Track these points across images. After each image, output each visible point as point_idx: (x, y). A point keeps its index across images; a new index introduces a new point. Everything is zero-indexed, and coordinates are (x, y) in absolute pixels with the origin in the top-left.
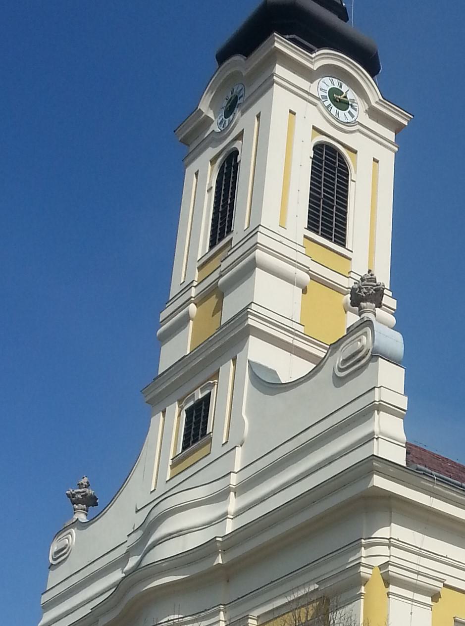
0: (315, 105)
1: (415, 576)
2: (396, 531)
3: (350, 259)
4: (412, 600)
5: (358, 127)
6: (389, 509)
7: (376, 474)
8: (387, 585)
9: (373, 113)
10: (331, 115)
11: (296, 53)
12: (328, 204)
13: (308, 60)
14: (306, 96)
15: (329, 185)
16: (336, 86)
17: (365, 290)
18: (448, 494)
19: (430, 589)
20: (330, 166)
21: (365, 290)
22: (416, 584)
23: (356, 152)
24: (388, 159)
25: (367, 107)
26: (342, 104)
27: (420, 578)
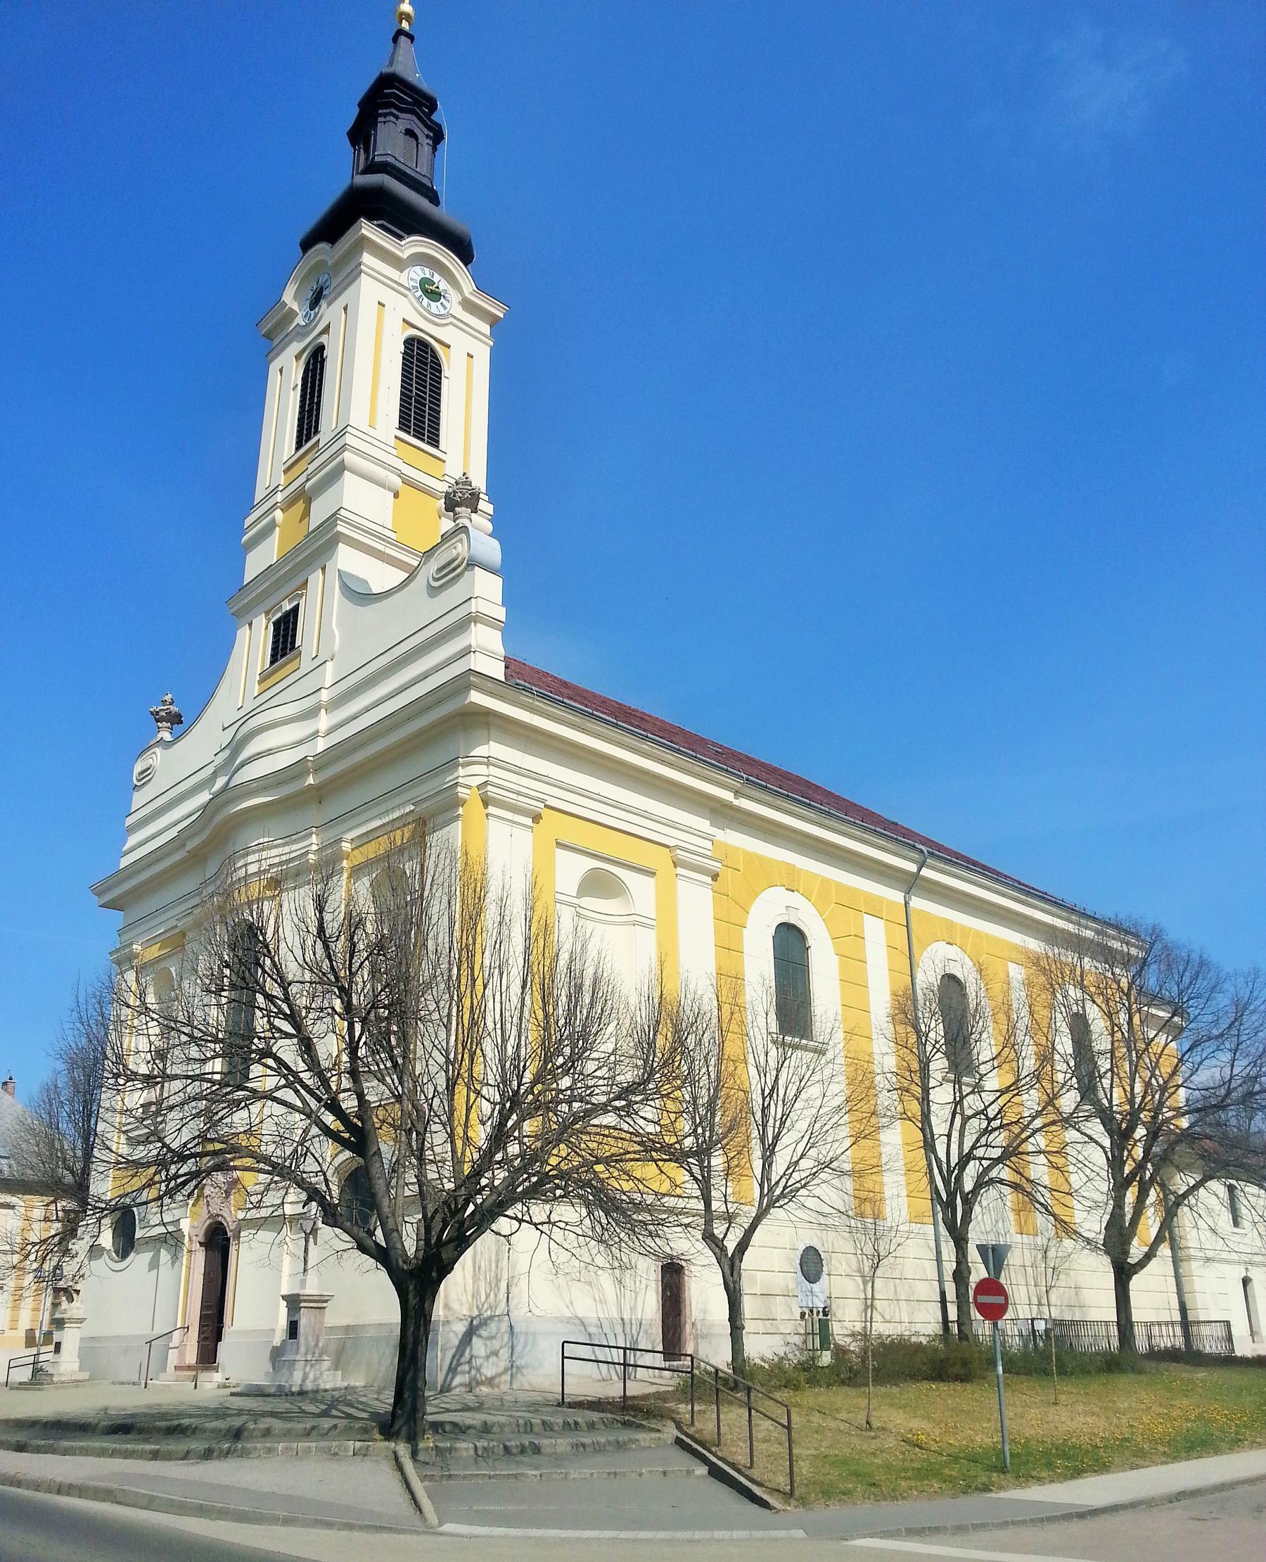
0: (405, 296)
1: (514, 796)
2: (494, 749)
3: (444, 462)
6: (488, 726)
9: (468, 305)
10: (423, 307)
15: (421, 382)
17: (460, 494)
21: (460, 494)
23: (449, 347)
27: (520, 798)
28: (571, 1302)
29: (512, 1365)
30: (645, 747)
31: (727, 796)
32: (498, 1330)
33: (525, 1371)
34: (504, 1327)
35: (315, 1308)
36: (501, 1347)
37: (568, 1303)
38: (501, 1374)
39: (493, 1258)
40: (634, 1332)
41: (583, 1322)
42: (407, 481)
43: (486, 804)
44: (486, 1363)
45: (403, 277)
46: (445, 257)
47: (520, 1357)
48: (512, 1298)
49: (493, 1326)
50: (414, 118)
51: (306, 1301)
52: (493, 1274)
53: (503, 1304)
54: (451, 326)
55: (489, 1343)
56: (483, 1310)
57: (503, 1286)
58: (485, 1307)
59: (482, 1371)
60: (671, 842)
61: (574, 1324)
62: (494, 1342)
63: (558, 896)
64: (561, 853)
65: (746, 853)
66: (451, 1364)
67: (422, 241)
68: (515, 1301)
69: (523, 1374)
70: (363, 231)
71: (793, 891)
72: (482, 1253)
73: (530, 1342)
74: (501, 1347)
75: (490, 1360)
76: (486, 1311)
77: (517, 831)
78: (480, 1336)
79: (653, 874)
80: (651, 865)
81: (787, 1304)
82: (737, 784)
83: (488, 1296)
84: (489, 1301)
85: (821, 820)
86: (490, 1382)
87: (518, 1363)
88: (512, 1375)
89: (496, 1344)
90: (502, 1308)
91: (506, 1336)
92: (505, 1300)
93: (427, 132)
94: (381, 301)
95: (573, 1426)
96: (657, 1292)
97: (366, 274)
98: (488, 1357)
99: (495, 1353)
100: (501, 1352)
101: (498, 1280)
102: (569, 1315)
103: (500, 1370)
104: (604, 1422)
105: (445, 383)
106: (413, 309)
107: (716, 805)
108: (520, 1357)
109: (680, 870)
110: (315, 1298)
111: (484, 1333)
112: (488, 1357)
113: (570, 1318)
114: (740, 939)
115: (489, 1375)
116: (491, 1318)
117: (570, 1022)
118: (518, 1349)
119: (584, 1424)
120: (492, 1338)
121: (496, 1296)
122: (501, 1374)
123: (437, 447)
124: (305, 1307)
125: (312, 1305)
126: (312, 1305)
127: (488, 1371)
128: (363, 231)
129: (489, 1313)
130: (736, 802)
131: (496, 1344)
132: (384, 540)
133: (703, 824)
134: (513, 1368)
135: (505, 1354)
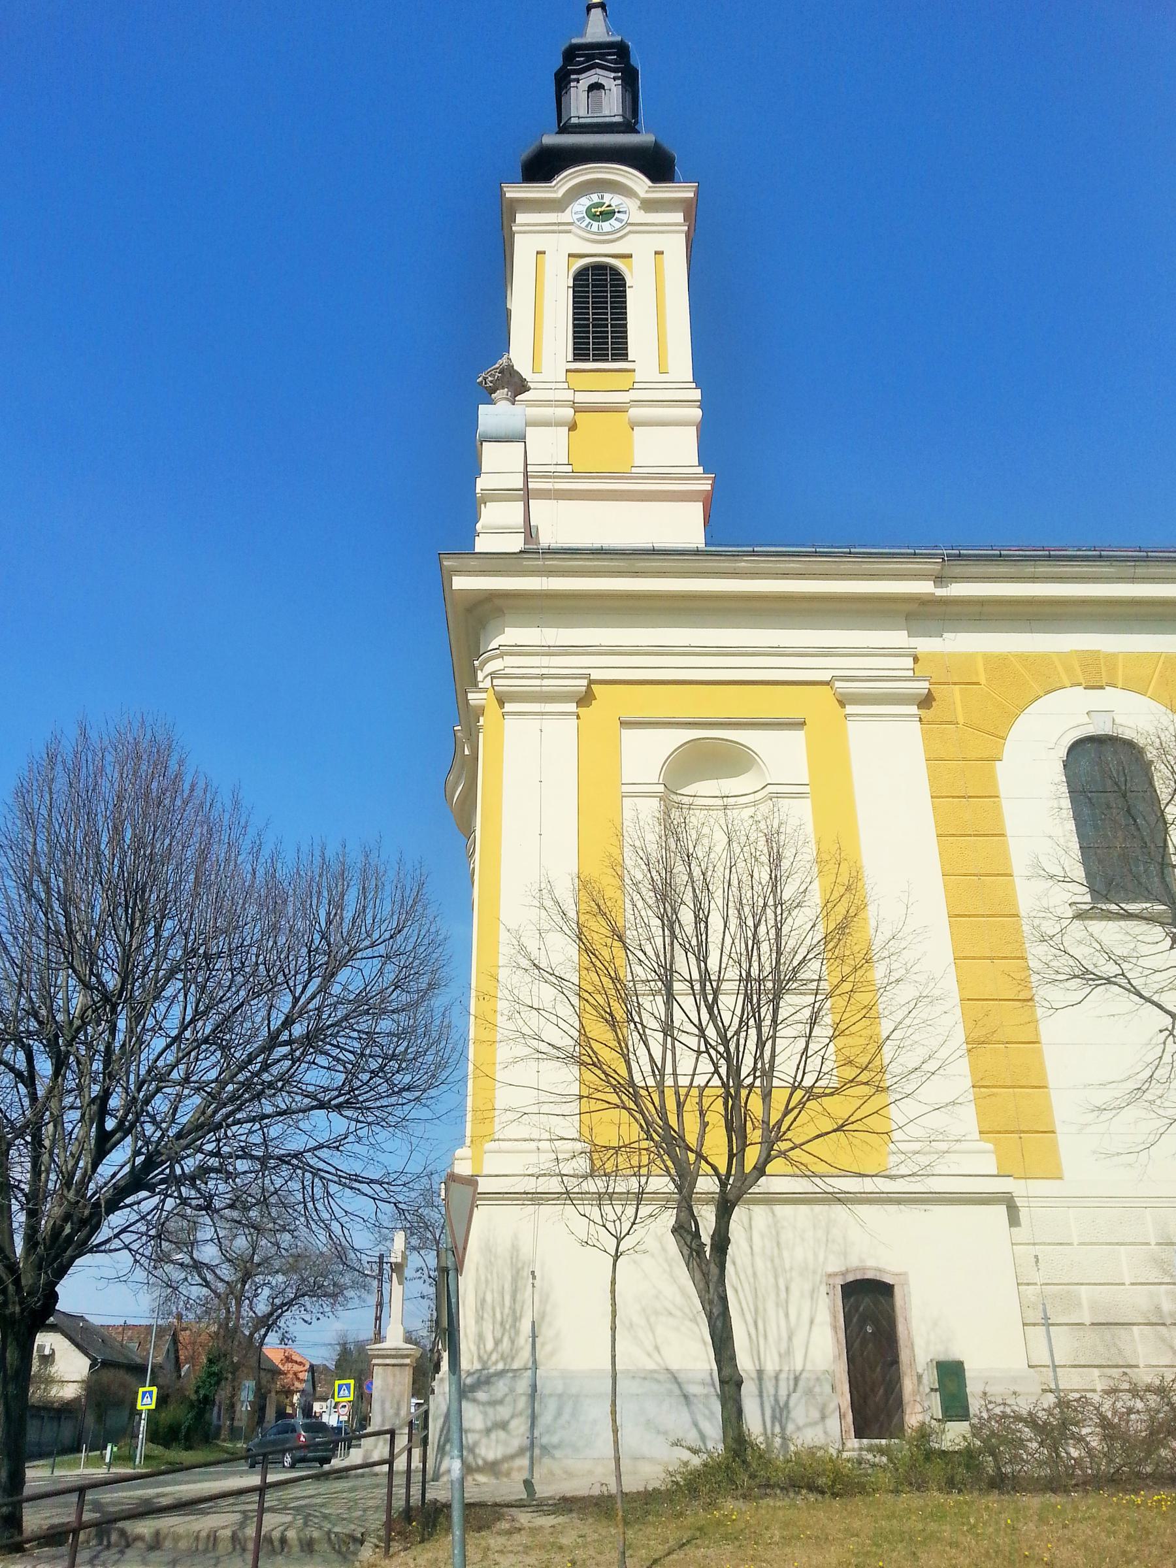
0: (569, 232)
1: (537, 682)
2: (511, 635)
3: (634, 371)
4: (543, 714)
5: (629, 228)
6: (500, 612)
7: (455, 575)
8: (502, 707)
9: (649, 205)
10: (594, 233)
11: (519, 192)
12: (600, 324)
13: (551, 192)
14: (555, 228)
15: (599, 305)
16: (589, 203)
17: (490, 379)
18: (571, 566)
19: (912, 694)
20: (600, 285)
21: (490, 379)
22: (541, 692)
23: (630, 256)
24: (676, 247)
25: (639, 202)
26: (608, 215)
27: (546, 682)
28: (657, 1348)
29: (532, 1444)
30: (743, 564)
31: (925, 587)
32: (512, 1390)
33: (558, 1454)
34: (523, 1386)
35: (394, 1365)
36: (512, 1417)
37: (650, 1349)
38: (512, 1457)
39: (507, 1287)
40: (783, 1392)
41: (675, 1378)
42: (579, 409)
43: (501, 702)
44: (484, 1441)
45: (566, 217)
46: (601, 172)
47: (549, 1431)
48: (543, 1344)
49: (501, 1388)
50: (598, 71)
51: (378, 1357)
52: (507, 1311)
53: (526, 1354)
54: (631, 236)
55: (490, 1410)
56: (490, 1363)
57: (525, 1327)
58: (494, 1357)
59: (477, 1451)
60: (826, 676)
61: (658, 1381)
62: (500, 1408)
63: (625, 788)
64: (627, 733)
65: (988, 658)
66: (439, 1442)
67: (575, 172)
68: (548, 1348)
69: (553, 1457)
70: (508, 195)
71: (1102, 688)
72: (487, 1281)
73: (567, 1410)
74: (512, 1417)
75: (493, 1436)
76: (496, 1363)
77: (549, 724)
78: (475, 1400)
79: (800, 725)
80: (794, 714)
81: (1163, 1340)
82: (933, 566)
83: (497, 1343)
84: (500, 1349)
85: (1130, 571)
86: (492, 1468)
87: (545, 1440)
88: (532, 1458)
89: (504, 1412)
90: (525, 1356)
91: (522, 1403)
92: (529, 1347)
93: (613, 75)
94: (539, 249)
95: (276, 1544)
96: (835, 1328)
97: (520, 232)
98: (488, 1431)
99: (503, 1426)
100: (514, 1424)
101: (516, 1319)
102: (651, 1365)
103: (511, 1450)
104: (330, 1538)
105: (630, 294)
106: (578, 240)
107: (914, 607)
108: (548, 1432)
109: (850, 709)
110: (389, 1352)
111: (481, 1395)
112: (488, 1431)
113: (652, 1371)
114: (992, 778)
115: (491, 1456)
116: (501, 1374)
117: (206, 921)
118: (545, 1419)
119: (296, 1543)
120: (493, 1403)
121: (513, 1342)
122: (512, 1457)
123: (626, 360)
124: (379, 1365)
125: (388, 1361)
126: (388, 1361)
127: (490, 1450)
128: (508, 195)
129: (500, 1366)
130: (941, 592)
131: (504, 1412)
132: (550, 477)
133: (898, 638)
134: (532, 1448)
135: (519, 1426)
